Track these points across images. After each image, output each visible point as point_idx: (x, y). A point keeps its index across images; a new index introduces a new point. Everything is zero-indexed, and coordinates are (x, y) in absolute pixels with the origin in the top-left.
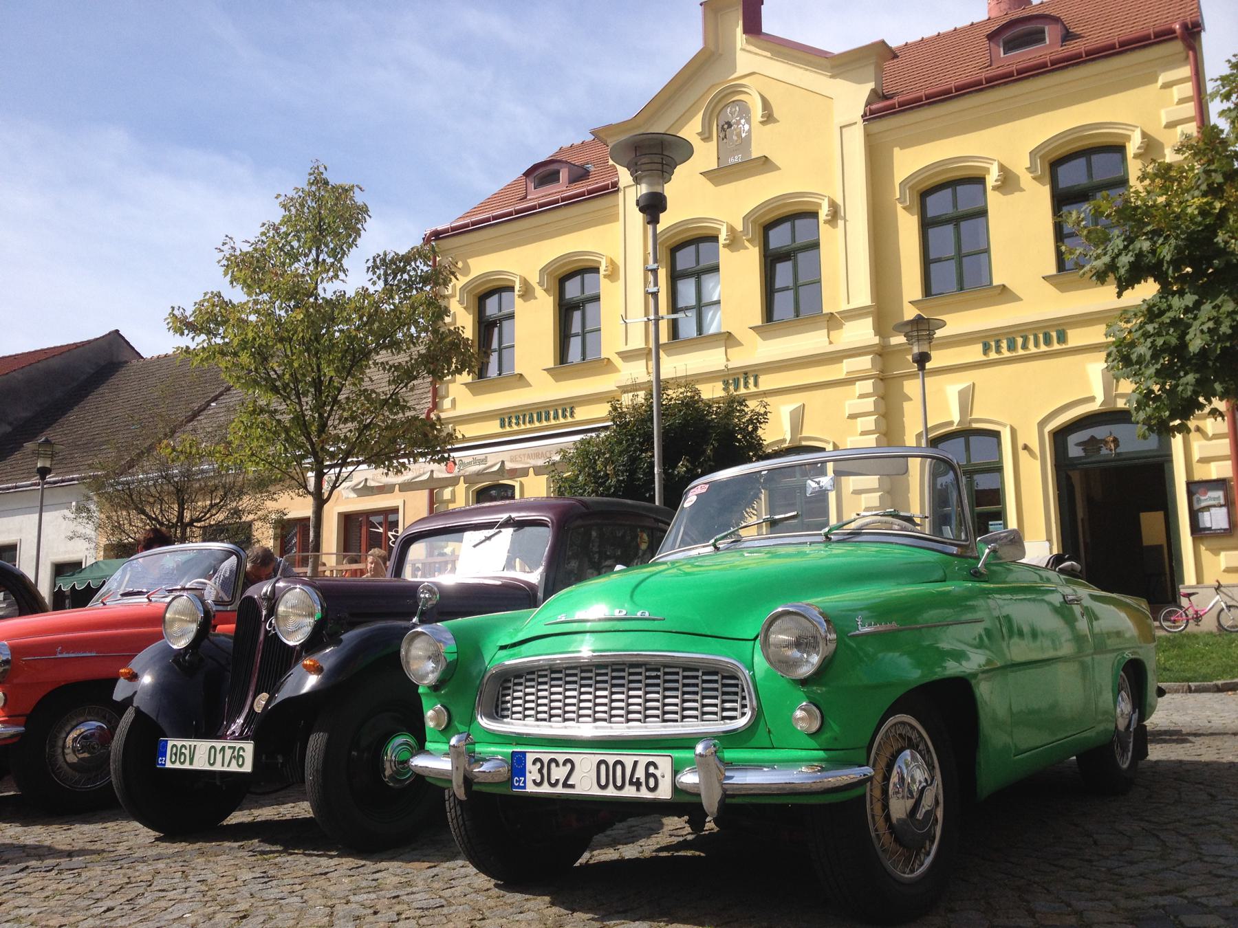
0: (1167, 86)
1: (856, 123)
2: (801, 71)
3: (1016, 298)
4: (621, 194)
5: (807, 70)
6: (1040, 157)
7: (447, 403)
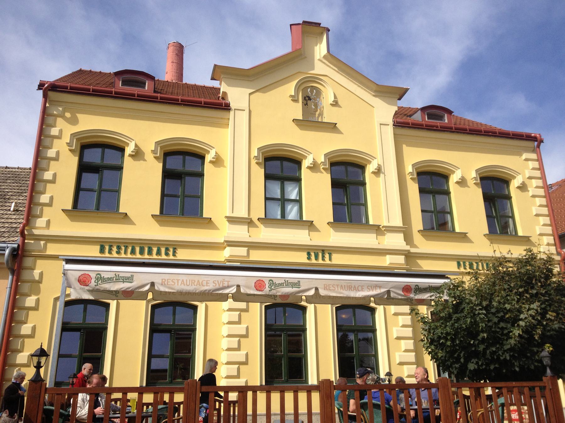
0: (527, 160)
1: (389, 125)
2: (356, 86)
3: (132, 223)
4: (232, 113)
5: (359, 86)
6: (77, 139)
7: (40, 222)
